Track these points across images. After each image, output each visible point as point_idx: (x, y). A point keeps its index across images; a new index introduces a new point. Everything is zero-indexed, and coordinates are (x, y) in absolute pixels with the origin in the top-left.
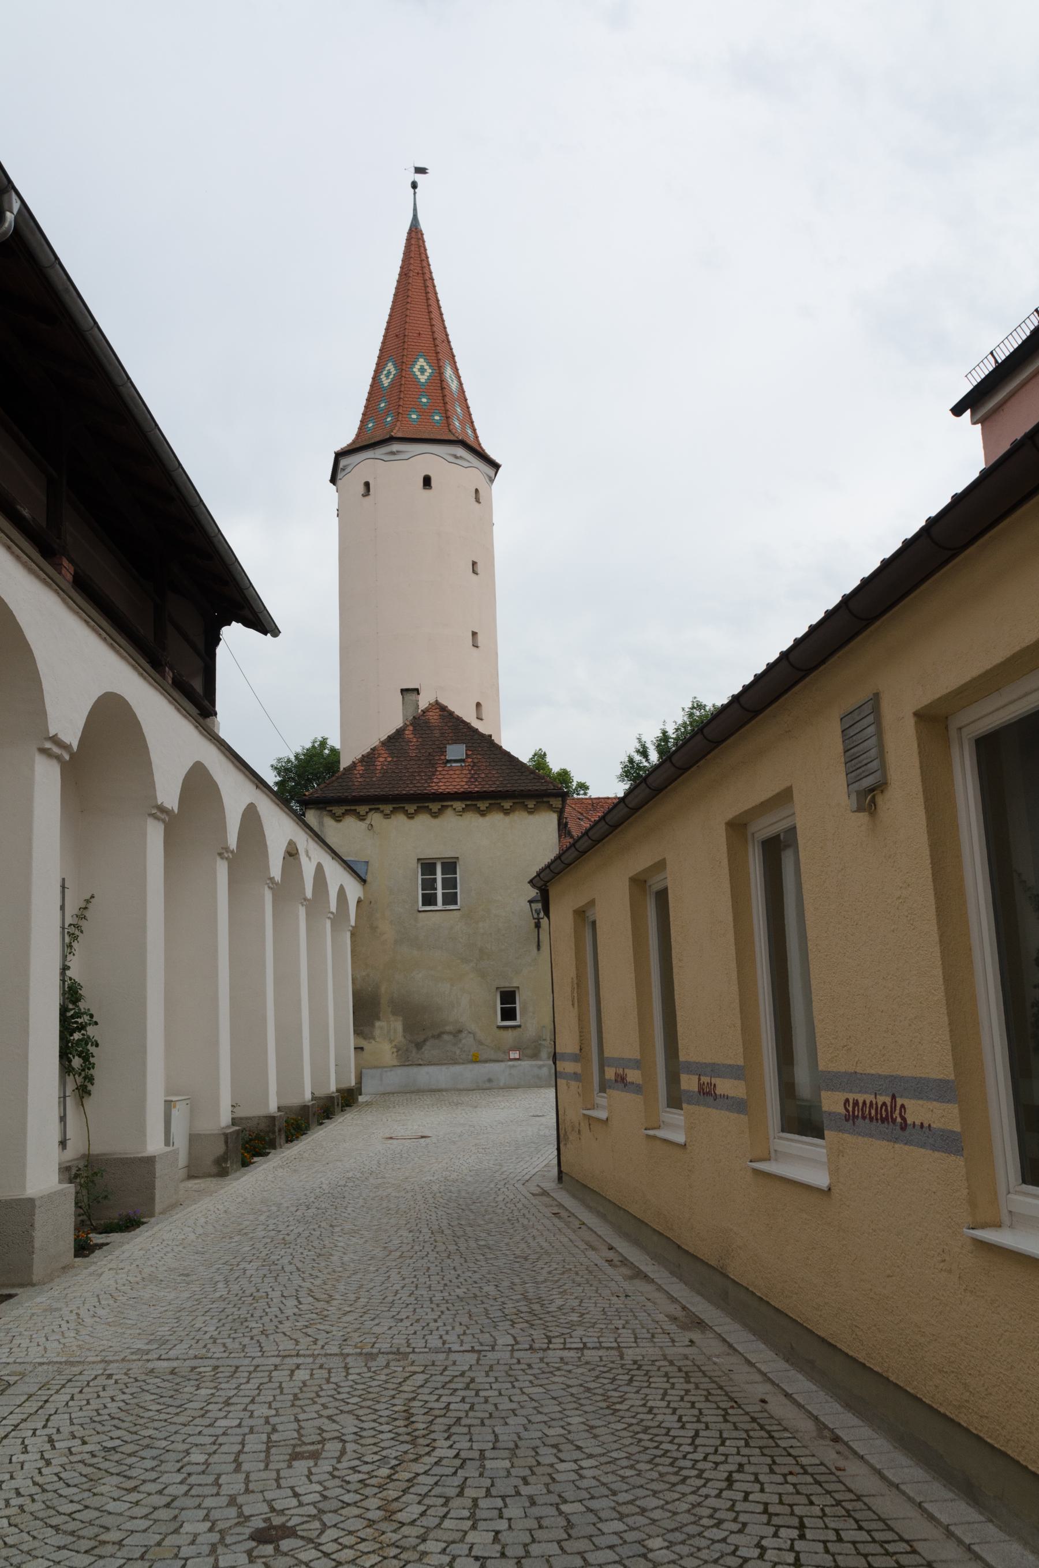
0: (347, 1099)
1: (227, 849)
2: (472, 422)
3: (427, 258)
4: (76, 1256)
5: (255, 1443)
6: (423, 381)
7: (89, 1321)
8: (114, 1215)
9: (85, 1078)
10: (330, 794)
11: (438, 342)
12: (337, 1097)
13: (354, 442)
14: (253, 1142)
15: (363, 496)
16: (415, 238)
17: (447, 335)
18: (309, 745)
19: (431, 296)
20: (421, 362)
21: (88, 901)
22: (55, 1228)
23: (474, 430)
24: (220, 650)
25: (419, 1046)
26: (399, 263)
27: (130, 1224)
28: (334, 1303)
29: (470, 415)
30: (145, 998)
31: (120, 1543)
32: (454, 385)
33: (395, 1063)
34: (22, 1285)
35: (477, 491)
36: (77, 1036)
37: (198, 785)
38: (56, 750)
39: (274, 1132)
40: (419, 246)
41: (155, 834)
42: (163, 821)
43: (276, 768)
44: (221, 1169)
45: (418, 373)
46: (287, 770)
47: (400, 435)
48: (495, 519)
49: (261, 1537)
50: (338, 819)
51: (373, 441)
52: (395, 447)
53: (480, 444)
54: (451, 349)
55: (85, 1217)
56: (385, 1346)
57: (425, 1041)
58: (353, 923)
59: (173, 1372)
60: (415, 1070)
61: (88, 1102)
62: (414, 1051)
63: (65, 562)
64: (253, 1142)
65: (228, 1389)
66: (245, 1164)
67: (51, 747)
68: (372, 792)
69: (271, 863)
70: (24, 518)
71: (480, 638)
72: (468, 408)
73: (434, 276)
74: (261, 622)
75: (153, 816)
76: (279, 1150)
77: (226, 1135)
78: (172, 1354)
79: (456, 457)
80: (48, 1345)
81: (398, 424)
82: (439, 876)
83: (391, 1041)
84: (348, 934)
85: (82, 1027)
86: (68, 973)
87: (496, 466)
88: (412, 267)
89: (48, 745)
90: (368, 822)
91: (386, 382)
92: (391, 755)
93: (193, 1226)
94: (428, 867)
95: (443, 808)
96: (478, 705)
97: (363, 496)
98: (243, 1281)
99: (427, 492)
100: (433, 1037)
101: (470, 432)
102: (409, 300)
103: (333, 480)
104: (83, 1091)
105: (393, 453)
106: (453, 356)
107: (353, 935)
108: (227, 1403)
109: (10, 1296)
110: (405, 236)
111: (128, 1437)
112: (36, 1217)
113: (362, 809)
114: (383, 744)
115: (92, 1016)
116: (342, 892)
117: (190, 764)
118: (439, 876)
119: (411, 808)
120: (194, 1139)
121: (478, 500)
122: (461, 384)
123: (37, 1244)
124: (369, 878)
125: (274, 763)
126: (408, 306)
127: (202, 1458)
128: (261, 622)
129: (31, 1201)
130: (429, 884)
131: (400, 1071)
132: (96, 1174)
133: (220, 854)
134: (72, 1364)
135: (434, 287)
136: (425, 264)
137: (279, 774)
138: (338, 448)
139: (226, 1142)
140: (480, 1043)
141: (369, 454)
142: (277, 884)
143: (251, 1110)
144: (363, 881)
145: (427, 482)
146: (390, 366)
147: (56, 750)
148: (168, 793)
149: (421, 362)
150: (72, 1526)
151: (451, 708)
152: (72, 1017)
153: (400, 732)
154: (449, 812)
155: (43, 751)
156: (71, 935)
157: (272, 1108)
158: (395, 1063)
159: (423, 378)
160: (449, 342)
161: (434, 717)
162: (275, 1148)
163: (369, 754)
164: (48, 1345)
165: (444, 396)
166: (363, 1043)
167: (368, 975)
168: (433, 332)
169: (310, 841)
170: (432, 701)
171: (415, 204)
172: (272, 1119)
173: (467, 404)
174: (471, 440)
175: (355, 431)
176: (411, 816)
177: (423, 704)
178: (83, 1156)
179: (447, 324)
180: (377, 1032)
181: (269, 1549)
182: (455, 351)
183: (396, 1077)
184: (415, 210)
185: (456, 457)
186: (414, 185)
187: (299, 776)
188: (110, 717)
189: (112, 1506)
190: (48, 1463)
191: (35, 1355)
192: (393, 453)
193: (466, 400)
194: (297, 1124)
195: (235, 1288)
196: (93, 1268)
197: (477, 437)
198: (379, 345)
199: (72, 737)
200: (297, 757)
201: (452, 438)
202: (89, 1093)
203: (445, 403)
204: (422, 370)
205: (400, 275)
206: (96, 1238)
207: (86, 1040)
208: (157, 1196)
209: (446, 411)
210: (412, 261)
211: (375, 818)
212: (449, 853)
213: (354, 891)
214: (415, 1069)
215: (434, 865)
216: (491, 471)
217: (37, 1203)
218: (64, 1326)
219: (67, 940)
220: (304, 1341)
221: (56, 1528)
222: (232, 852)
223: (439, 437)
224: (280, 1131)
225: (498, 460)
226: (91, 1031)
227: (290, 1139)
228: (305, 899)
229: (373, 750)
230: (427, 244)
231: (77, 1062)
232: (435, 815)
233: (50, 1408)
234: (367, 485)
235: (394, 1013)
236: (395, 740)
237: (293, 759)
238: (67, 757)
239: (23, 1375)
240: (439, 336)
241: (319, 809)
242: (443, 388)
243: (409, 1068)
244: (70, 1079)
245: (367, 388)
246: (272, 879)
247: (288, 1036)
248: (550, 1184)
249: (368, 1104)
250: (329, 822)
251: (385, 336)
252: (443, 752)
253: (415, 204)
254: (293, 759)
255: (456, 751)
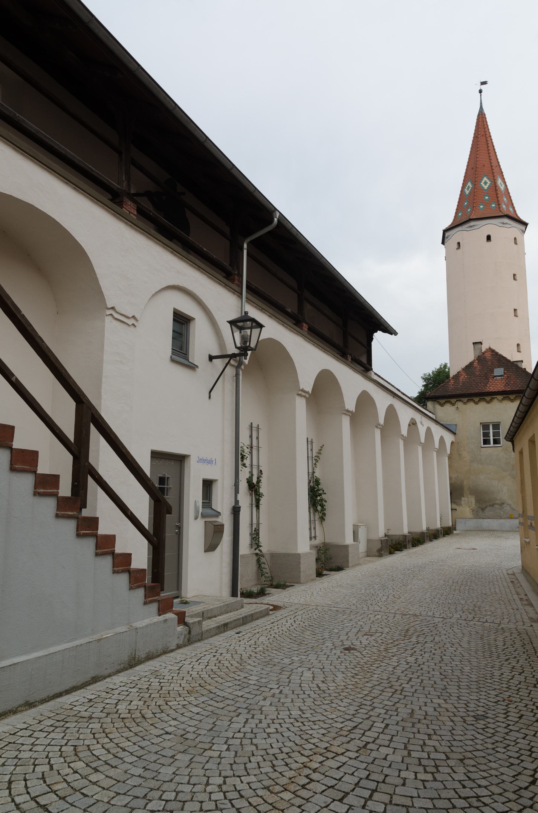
0: (447, 531)
1: (379, 425)
2: (513, 204)
3: (488, 126)
4: (317, 577)
5: (355, 630)
6: (486, 188)
7: (315, 595)
8: (334, 566)
9: (323, 514)
10: (438, 394)
11: (493, 168)
12: (441, 530)
13: (452, 224)
14: (394, 545)
15: (457, 249)
16: (481, 118)
17: (498, 163)
18: (438, 367)
19: (490, 145)
20: (485, 179)
21: (321, 447)
22: (309, 566)
23: (514, 208)
24: (373, 343)
25: (483, 510)
26: (473, 132)
27: (339, 569)
28: (401, 599)
29: (511, 201)
30: (343, 484)
31: (307, 644)
32: (502, 188)
33: (472, 516)
34: (297, 583)
35: (515, 238)
36: (319, 498)
37: (365, 400)
38: (303, 394)
39: (406, 542)
40: (483, 121)
41: (346, 421)
42: (349, 415)
43: (424, 378)
44: (380, 554)
45: (488, 181)
46: (430, 379)
47: (474, 217)
48: (526, 251)
49: (346, 649)
50: (442, 405)
51: (461, 222)
52: (472, 223)
53: (517, 215)
54: (501, 169)
55: (323, 565)
56: (411, 613)
57: (486, 507)
58: (449, 452)
59: (337, 611)
60: (481, 521)
61: (324, 523)
62: (481, 512)
63: (304, 325)
64: (394, 545)
65: (352, 617)
66: (391, 553)
67: (302, 393)
68: (458, 392)
69: (402, 429)
70: (289, 312)
71: (519, 312)
72: (510, 197)
73: (492, 134)
74: (388, 330)
75: (345, 414)
76: (408, 549)
77: (381, 541)
78: (338, 606)
79: (503, 223)
80: (301, 599)
81: (474, 212)
82: (491, 431)
83: (470, 507)
84: (447, 458)
85: (320, 495)
86: (315, 474)
87: (526, 224)
88: (479, 133)
89: (300, 393)
90: (456, 406)
91: (467, 192)
92: (467, 374)
93: (362, 573)
94: (485, 426)
95: (491, 400)
96: (518, 345)
97: (457, 249)
98: (372, 590)
99: (489, 243)
100: (490, 505)
101: (511, 209)
102: (478, 149)
103: (443, 243)
104: (322, 519)
105: (471, 227)
106: (502, 173)
107: (450, 458)
108: (351, 620)
109: (293, 586)
110: (476, 117)
111: (317, 623)
112: (301, 560)
113: (453, 401)
114: (463, 369)
115: (323, 491)
116: (442, 439)
117: (359, 392)
118: (491, 431)
119: (477, 399)
120: (369, 541)
121: (516, 243)
122: (506, 186)
123: (302, 569)
124: (457, 432)
125: (423, 375)
126: (478, 153)
127: (337, 631)
128: (388, 330)
129: (299, 554)
130: (486, 435)
131: (474, 521)
132: (327, 550)
133: (376, 427)
134: (307, 605)
135: (492, 140)
136: (486, 130)
137: (425, 381)
138: (444, 228)
139: (382, 543)
140: (513, 509)
141: (460, 228)
142: (405, 437)
143: (395, 532)
144: (455, 434)
145: (489, 238)
146: (469, 184)
147: (303, 394)
148: (350, 404)
149: (485, 179)
150: (295, 639)
151: (497, 350)
152: (317, 491)
153: (471, 364)
154: (495, 401)
155: (299, 395)
156: (315, 460)
157: (406, 531)
158: (472, 516)
159: (486, 187)
160: (500, 166)
161: (488, 355)
162: (406, 548)
163: (456, 375)
164: (301, 599)
165: (497, 194)
166: (455, 507)
167: (458, 476)
168: (491, 163)
169: (423, 417)
170: (488, 347)
171: (481, 101)
172: (405, 536)
173: (510, 196)
174: (512, 214)
175: (453, 218)
176: (476, 403)
177: (484, 350)
178: (323, 543)
179: (498, 157)
180: (463, 502)
181: (347, 652)
182: (503, 170)
183: (473, 523)
184: (481, 103)
185: (503, 223)
186: (480, 91)
187: (435, 382)
188: (325, 380)
189: (307, 637)
190: (292, 626)
191: (296, 601)
192: (471, 227)
193: (509, 193)
194: (418, 540)
195: (368, 591)
196: (321, 581)
197: (515, 211)
198: (463, 175)
199: (309, 389)
200: (433, 372)
201: (501, 214)
202: (324, 520)
203: (498, 197)
204: (485, 183)
205: (474, 138)
206: (325, 572)
207: (322, 500)
208: (350, 560)
209: (498, 201)
210: (480, 130)
211: (460, 404)
212: (496, 420)
213: (449, 438)
214: (482, 520)
215: (489, 425)
216: (523, 228)
217: (301, 555)
218: (307, 595)
219: (314, 462)
220: (384, 608)
221: (291, 639)
222: (382, 425)
223: (494, 215)
224: (409, 541)
225: (527, 221)
226: (324, 496)
227: (414, 545)
228: (421, 443)
229: (458, 373)
230: (487, 120)
231: (319, 508)
232: (488, 402)
233: (297, 614)
234: (459, 244)
235: (470, 494)
236: (469, 367)
237: (431, 374)
238: (308, 396)
239: (291, 606)
240: (494, 164)
241: (433, 401)
242: (496, 190)
243: (479, 520)
244: (317, 514)
245: (458, 197)
246: (403, 435)
247: (413, 503)
248: (518, 571)
249: (457, 534)
250: (438, 407)
251: (467, 170)
252: (493, 372)
253: (481, 101)
254: (431, 374)
255: (499, 371)
